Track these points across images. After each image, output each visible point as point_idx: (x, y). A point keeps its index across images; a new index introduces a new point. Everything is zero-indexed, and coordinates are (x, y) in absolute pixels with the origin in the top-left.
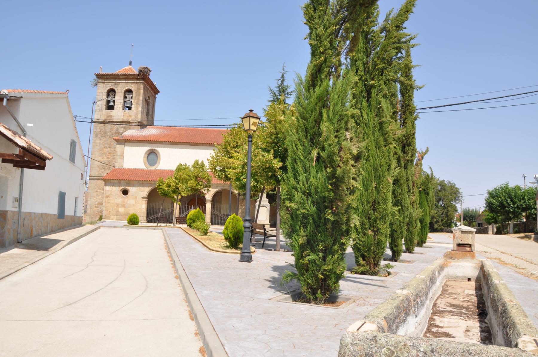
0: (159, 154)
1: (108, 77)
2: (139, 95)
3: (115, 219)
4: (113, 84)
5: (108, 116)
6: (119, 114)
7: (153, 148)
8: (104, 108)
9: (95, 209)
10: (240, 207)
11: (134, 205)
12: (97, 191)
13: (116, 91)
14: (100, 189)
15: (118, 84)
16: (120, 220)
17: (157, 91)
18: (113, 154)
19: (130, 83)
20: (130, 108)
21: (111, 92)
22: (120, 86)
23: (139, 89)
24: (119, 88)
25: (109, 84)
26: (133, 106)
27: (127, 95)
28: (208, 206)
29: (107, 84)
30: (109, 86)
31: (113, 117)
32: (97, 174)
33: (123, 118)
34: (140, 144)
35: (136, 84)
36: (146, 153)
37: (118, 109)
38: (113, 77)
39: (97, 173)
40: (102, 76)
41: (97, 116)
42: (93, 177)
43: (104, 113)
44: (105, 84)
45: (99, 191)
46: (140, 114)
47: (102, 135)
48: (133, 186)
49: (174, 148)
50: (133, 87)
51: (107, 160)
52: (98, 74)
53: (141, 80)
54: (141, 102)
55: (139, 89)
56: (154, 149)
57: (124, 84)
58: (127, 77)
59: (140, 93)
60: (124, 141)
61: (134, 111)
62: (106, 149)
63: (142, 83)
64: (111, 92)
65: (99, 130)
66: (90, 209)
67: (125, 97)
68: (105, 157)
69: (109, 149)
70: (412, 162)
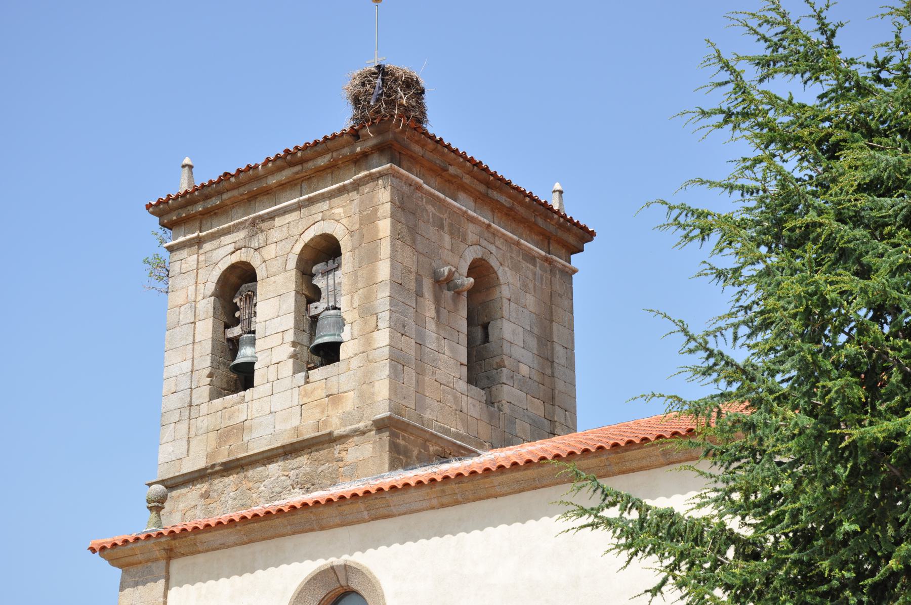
1: (210, 203)
2: (372, 257)
4: (241, 234)
5: (226, 434)
6: (278, 402)
7: (335, 561)
15: (265, 225)
17: (560, 226)
23: (369, 219)
24: (270, 252)
26: (346, 335)
29: (215, 243)
33: (295, 422)
34: (258, 547)
37: (272, 377)
38: (235, 193)
40: (183, 206)
43: (203, 423)
44: (207, 246)
46: (386, 371)
52: (159, 202)
53: (375, 158)
54: (383, 296)
55: (369, 219)
56: (346, 568)
59: (375, 241)
60: (157, 552)
61: (355, 363)
63: (381, 175)
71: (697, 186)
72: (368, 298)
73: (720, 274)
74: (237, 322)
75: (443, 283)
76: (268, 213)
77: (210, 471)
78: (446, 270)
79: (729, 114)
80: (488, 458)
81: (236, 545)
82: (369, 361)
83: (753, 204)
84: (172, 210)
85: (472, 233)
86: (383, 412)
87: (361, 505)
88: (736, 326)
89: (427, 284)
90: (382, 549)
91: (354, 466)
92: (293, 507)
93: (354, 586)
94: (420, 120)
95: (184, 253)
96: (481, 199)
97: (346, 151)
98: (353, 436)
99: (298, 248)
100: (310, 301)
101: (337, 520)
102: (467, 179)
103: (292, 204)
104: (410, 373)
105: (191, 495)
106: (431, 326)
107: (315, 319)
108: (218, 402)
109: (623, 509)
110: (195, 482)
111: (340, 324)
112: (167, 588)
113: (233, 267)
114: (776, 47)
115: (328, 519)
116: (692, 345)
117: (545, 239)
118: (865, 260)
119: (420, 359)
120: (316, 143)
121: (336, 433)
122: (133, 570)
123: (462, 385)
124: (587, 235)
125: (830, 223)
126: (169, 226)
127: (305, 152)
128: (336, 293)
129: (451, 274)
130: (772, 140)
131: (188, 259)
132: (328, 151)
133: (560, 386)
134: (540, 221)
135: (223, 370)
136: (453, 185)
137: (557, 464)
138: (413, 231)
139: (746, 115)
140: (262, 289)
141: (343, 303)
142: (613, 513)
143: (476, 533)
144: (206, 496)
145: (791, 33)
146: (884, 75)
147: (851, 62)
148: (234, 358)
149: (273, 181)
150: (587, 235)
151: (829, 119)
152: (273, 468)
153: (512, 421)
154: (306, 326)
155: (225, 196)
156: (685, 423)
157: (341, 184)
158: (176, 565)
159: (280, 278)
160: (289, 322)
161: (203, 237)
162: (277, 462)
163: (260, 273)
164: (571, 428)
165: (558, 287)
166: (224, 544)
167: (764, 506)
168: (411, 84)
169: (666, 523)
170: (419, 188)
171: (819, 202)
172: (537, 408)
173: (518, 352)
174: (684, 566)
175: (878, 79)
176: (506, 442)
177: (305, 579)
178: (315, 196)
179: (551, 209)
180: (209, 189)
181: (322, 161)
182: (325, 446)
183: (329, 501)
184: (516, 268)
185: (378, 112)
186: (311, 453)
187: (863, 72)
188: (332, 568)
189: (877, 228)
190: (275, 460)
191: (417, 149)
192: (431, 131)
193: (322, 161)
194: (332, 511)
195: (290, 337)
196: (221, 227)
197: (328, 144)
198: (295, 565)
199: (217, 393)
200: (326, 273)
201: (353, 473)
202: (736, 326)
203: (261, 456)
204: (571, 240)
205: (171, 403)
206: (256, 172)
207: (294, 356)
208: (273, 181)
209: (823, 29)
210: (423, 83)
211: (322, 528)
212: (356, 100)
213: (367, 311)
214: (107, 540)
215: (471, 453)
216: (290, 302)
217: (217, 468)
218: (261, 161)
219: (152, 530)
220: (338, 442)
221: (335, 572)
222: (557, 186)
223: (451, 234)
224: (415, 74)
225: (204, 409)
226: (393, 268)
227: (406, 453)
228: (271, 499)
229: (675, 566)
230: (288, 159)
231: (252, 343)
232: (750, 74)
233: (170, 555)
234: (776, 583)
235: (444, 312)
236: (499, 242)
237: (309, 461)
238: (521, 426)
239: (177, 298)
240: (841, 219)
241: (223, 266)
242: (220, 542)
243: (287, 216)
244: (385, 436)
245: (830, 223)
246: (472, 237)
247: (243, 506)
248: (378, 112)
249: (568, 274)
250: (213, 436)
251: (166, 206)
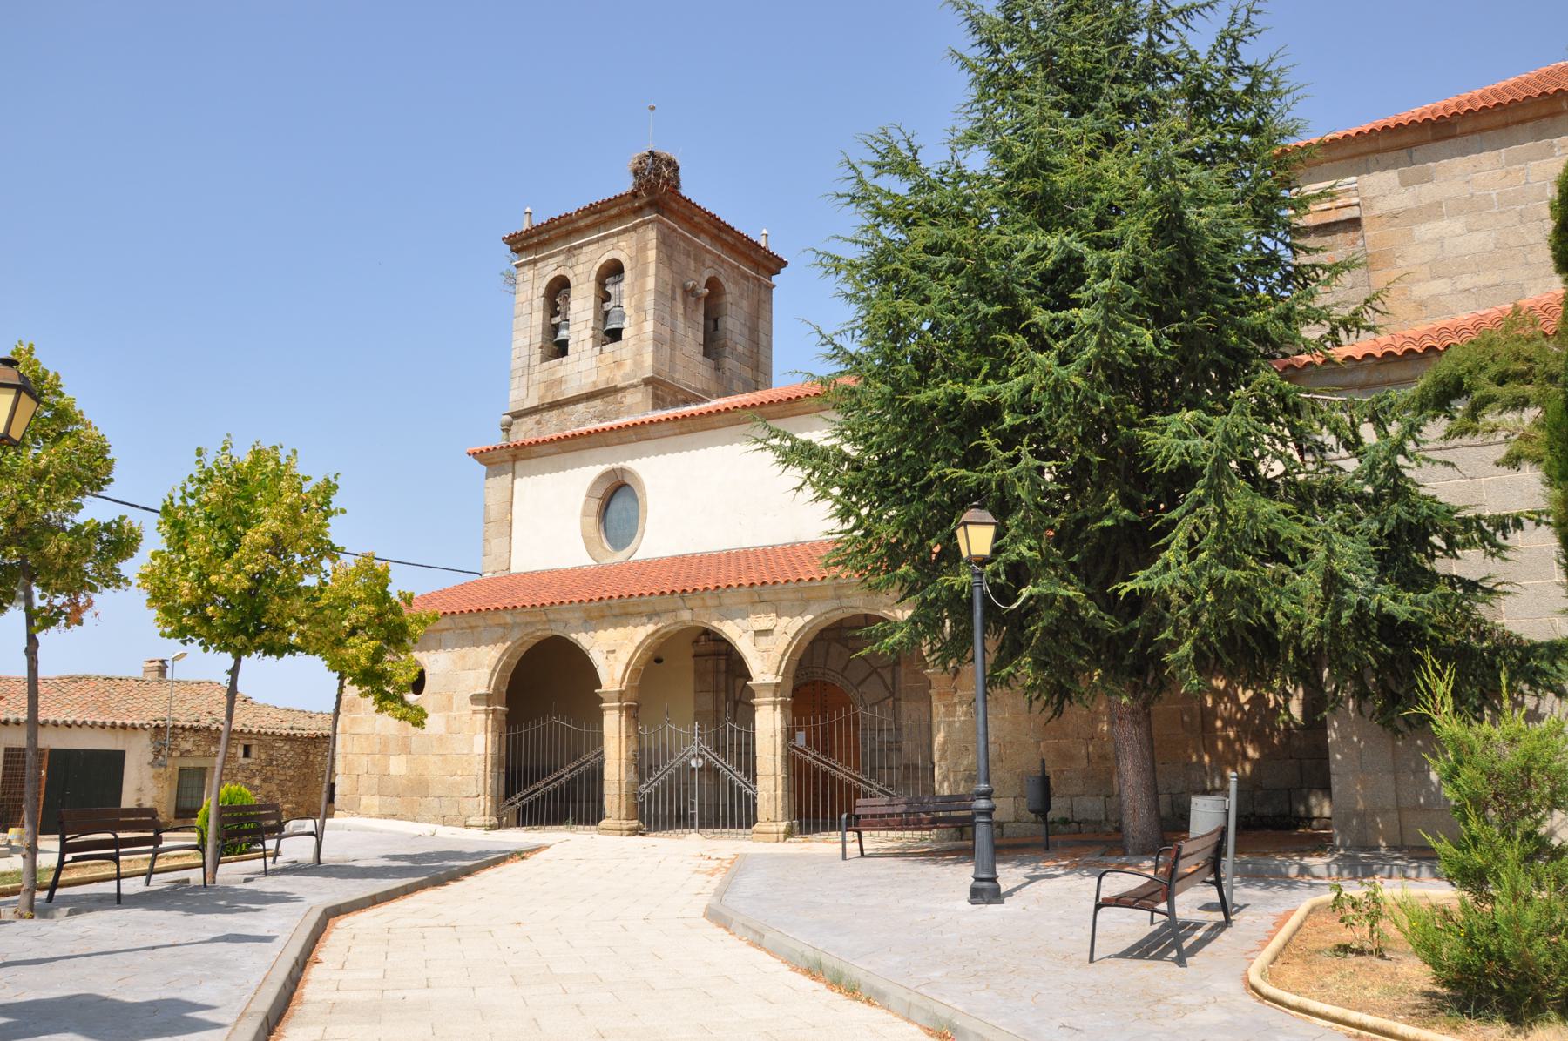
0: (642, 488)
1: (541, 238)
2: (643, 274)
3: (375, 811)
4: (561, 258)
7: (615, 465)
10: (939, 708)
11: (440, 738)
15: (576, 252)
16: (393, 816)
17: (766, 257)
19: (613, 235)
20: (615, 335)
21: (558, 290)
22: (582, 258)
23: (642, 250)
24: (579, 269)
25: (551, 261)
26: (626, 324)
28: (768, 723)
30: (550, 270)
33: (594, 378)
34: (568, 456)
35: (633, 233)
36: (590, 495)
37: (580, 349)
38: (558, 231)
43: (537, 377)
44: (540, 265)
46: (651, 348)
48: (440, 646)
49: (714, 446)
50: (621, 248)
53: (647, 210)
54: (650, 300)
55: (642, 250)
56: (622, 470)
58: (601, 216)
59: (646, 264)
60: (507, 457)
61: (631, 342)
63: (650, 221)
64: (558, 290)
71: (835, 240)
72: (641, 301)
73: (847, 296)
74: (558, 313)
75: (689, 292)
78: (691, 284)
79: (854, 198)
80: (716, 403)
82: (640, 341)
83: (866, 254)
84: (518, 241)
85: (708, 259)
86: (649, 374)
87: (631, 432)
88: (853, 330)
89: (679, 292)
90: (644, 459)
91: (630, 407)
92: (589, 432)
93: (627, 481)
94: (677, 186)
95: (526, 268)
96: (715, 239)
97: (629, 205)
99: (597, 267)
100: (604, 301)
102: (706, 226)
104: (666, 350)
105: (530, 422)
106: (680, 319)
107: (607, 313)
108: (546, 364)
109: (781, 440)
111: (623, 317)
112: (514, 479)
113: (556, 279)
114: (884, 157)
116: (824, 341)
117: (756, 265)
118: (926, 292)
119: (673, 340)
121: (620, 386)
122: (493, 467)
123: (700, 358)
124: (783, 264)
125: (906, 270)
126: (517, 251)
128: (620, 297)
129: (694, 286)
130: (878, 216)
131: (528, 273)
132: (617, 205)
133: (762, 359)
134: (753, 254)
135: (549, 344)
136: (697, 229)
137: (742, 412)
138: (670, 258)
139: (863, 198)
140: (573, 293)
141: (625, 303)
142: (775, 442)
143: (702, 451)
144: (538, 423)
145: (892, 148)
146: (945, 179)
147: (927, 170)
148: (556, 336)
149: (582, 223)
150: (783, 264)
151: (911, 204)
152: (580, 407)
153: (731, 381)
154: (601, 318)
156: (817, 388)
158: (518, 465)
159: (585, 286)
160: (590, 314)
163: (573, 283)
164: (769, 386)
165: (763, 296)
167: (866, 438)
168: (671, 163)
169: (807, 448)
170: (674, 230)
171: (900, 255)
172: (747, 373)
173: (737, 338)
174: (817, 475)
175: (942, 182)
176: (727, 394)
179: (760, 246)
181: (613, 212)
183: (612, 429)
184: (736, 283)
185: (649, 181)
187: (934, 177)
189: (934, 274)
191: (674, 205)
192: (683, 194)
193: (613, 212)
194: (613, 435)
195: (591, 324)
197: (617, 201)
198: (591, 467)
199: (545, 359)
200: (615, 284)
201: (630, 410)
202: (853, 330)
204: (773, 266)
205: (517, 364)
207: (593, 336)
208: (582, 223)
209: (911, 148)
210: (679, 163)
212: (635, 173)
213: (640, 309)
214: (477, 448)
215: (703, 401)
216: (591, 302)
218: (574, 211)
219: (504, 443)
222: (765, 232)
223: (695, 260)
224: (674, 157)
225: (537, 368)
226: (656, 281)
227: (663, 400)
228: (578, 426)
229: (809, 476)
230: (592, 210)
231: (567, 327)
232: (868, 173)
233: (515, 459)
234: (869, 485)
235: (689, 310)
236: (725, 266)
238: (737, 384)
239: (520, 297)
240: (914, 267)
241: (549, 278)
244: (650, 389)
245: (906, 270)
246: (708, 263)
247: (562, 430)
248: (649, 181)
249: (770, 288)
250: (543, 385)
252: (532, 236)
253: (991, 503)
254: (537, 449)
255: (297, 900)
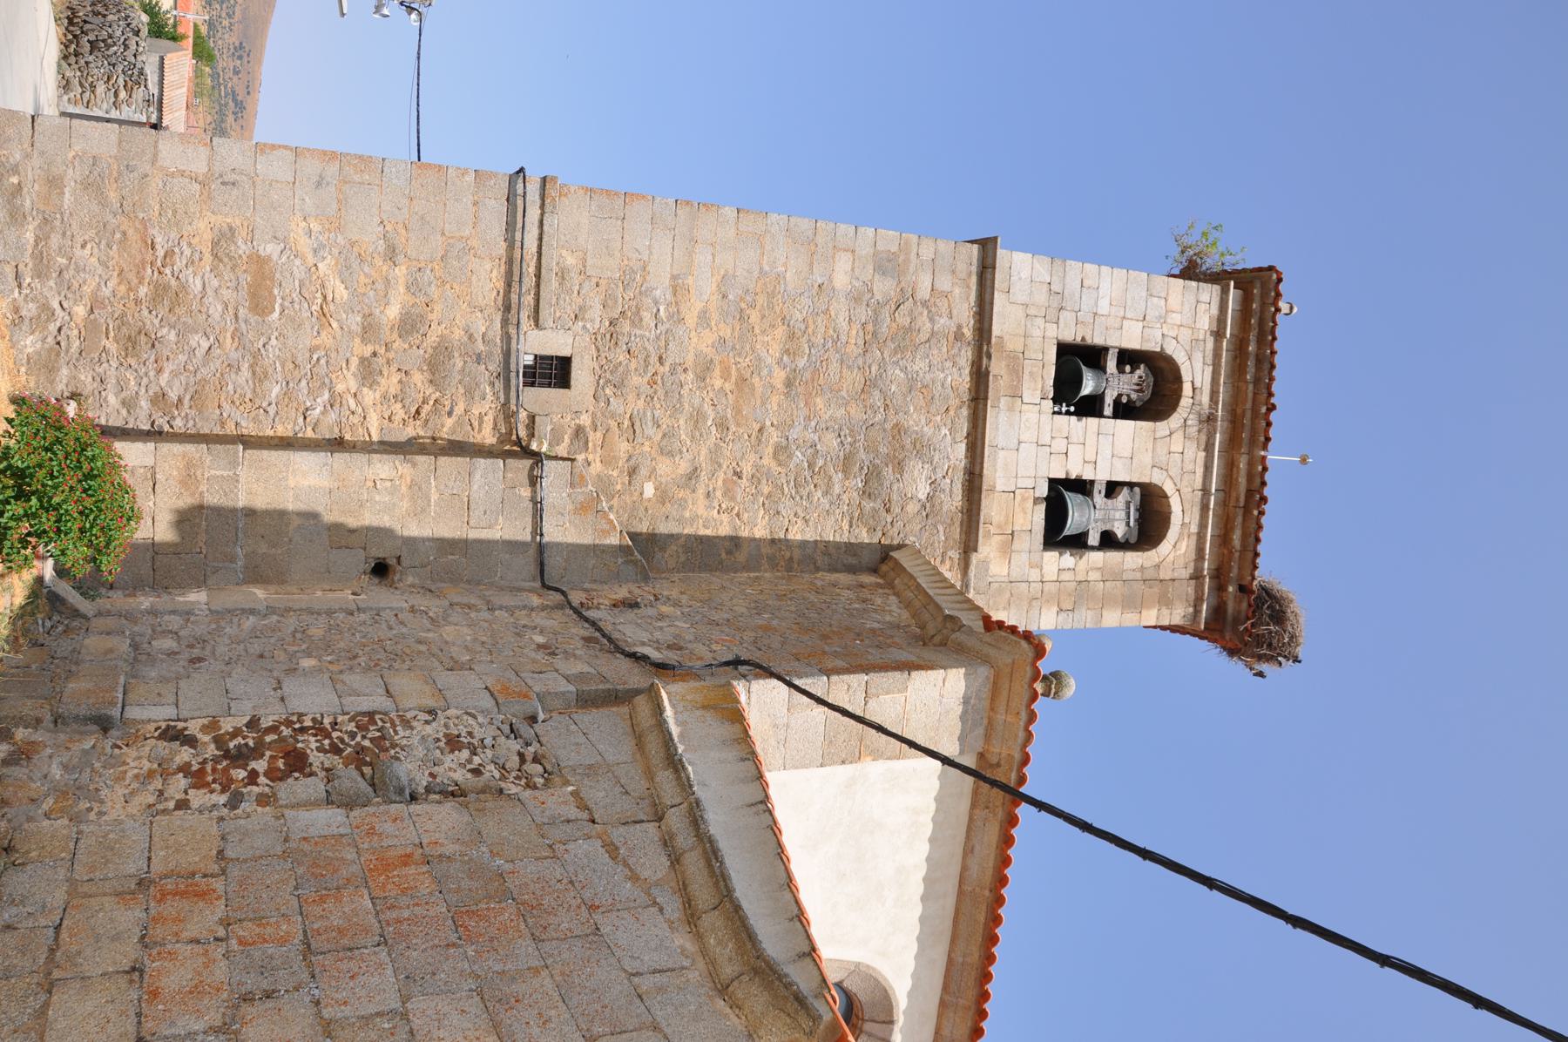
1: (1251, 363)
8: (1070, 335)
9: (203, 228)
12: (391, 254)
13: (1162, 427)
14: (413, 287)
15: (1203, 438)
18: (738, 411)
24: (1177, 443)
27: (1124, 494)
29: (1209, 360)
30: (1196, 373)
31: (1011, 409)
32: (560, 255)
33: (999, 487)
39: (570, 260)
41: (1025, 274)
42: (533, 213)
45: (400, 271)
47: (885, 314)
51: (690, 360)
57: (1198, 483)
62: (776, 349)
63: (1197, 611)
65: (924, 292)
66: (200, 167)
67: (1112, 488)
68: (709, 337)
69: (779, 376)
70: (924, 641)
76: (1214, 444)
77: (985, 348)
81: (964, 868)
97: (1234, 573)
98: (963, 581)
101: (946, 1032)
103: (1211, 482)
110: (977, 317)
115: (952, 1021)
120: (1258, 540)
127: (1254, 521)
155: (1251, 387)
157: (1207, 557)
161: (1222, 342)
162: (966, 457)
166: (972, 851)
177: (891, 987)
178: (1208, 517)
180: (1266, 372)
181: (1236, 537)
182: (963, 536)
186: (962, 513)
188: (891, 1022)
190: (969, 455)
193: (1236, 537)
196: (1223, 372)
197: (1251, 555)
203: (979, 437)
206: (1261, 445)
211: (943, 1004)
217: (985, 361)
220: (963, 555)
221: (884, 1022)
230: (1255, 498)
237: (953, 509)
242: (977, 848)
243: (1202, 470)
251: (1271, 301)
252: (1261, 341)
253: (240, 514)
254: (992, 834)
255: (16, 929)
